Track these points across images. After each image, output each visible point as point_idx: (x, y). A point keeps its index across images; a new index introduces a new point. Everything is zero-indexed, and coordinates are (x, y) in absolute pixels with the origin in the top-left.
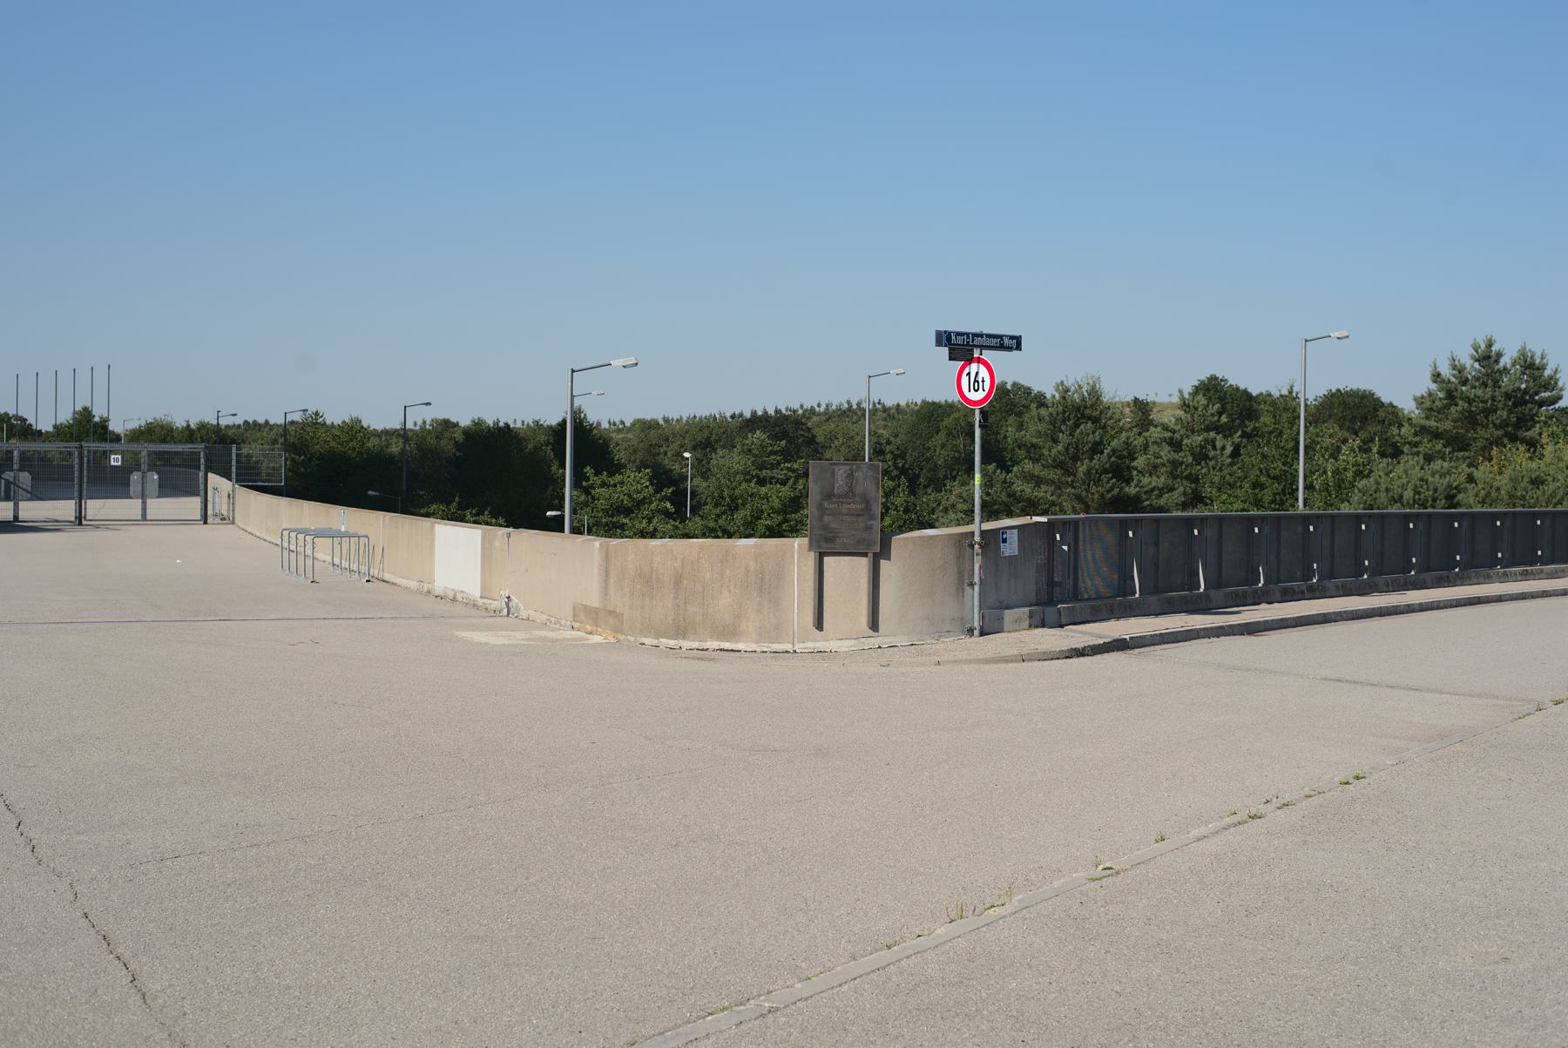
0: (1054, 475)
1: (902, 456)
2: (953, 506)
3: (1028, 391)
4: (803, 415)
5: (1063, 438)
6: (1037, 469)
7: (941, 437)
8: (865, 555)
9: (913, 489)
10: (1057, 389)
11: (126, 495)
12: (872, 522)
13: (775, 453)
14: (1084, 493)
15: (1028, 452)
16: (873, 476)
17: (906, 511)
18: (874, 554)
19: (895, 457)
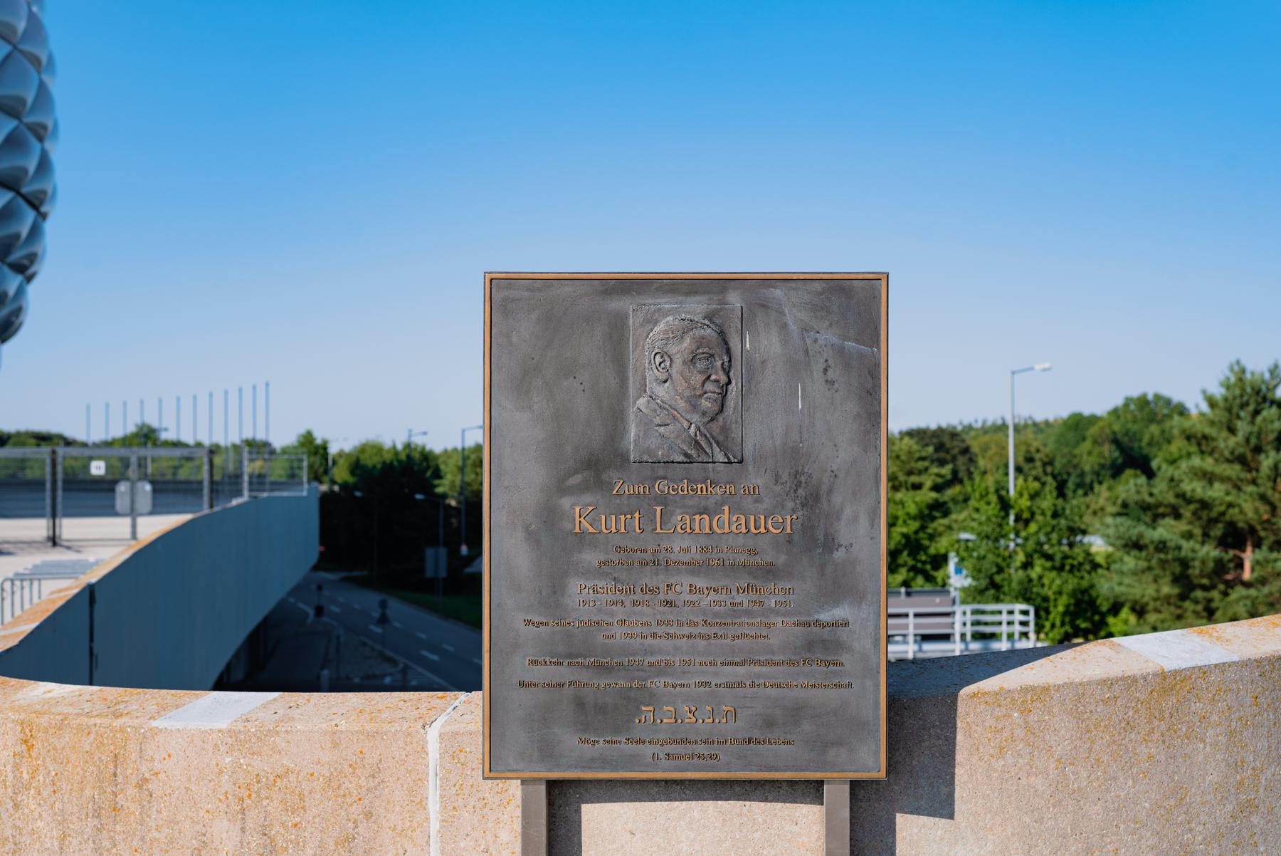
0: (1234, 470)
1: (1051, 463)
2: (1102, 509)
3: (1168, 402)
4: (963, 431)
5: (1243, 427)
6: (1208, 464)
7: (1087, 445)
8: (811, 791)
9: (1061, 491)
10: (1232, 369)
11: (111, 511)
12: (839, 613)
13: (923, 459)
14: (1270, 492)
15: (1199, 444)
16: (841, 351)
17: (1055, 515)
18: (855, 785)
19: (1045, 464)
